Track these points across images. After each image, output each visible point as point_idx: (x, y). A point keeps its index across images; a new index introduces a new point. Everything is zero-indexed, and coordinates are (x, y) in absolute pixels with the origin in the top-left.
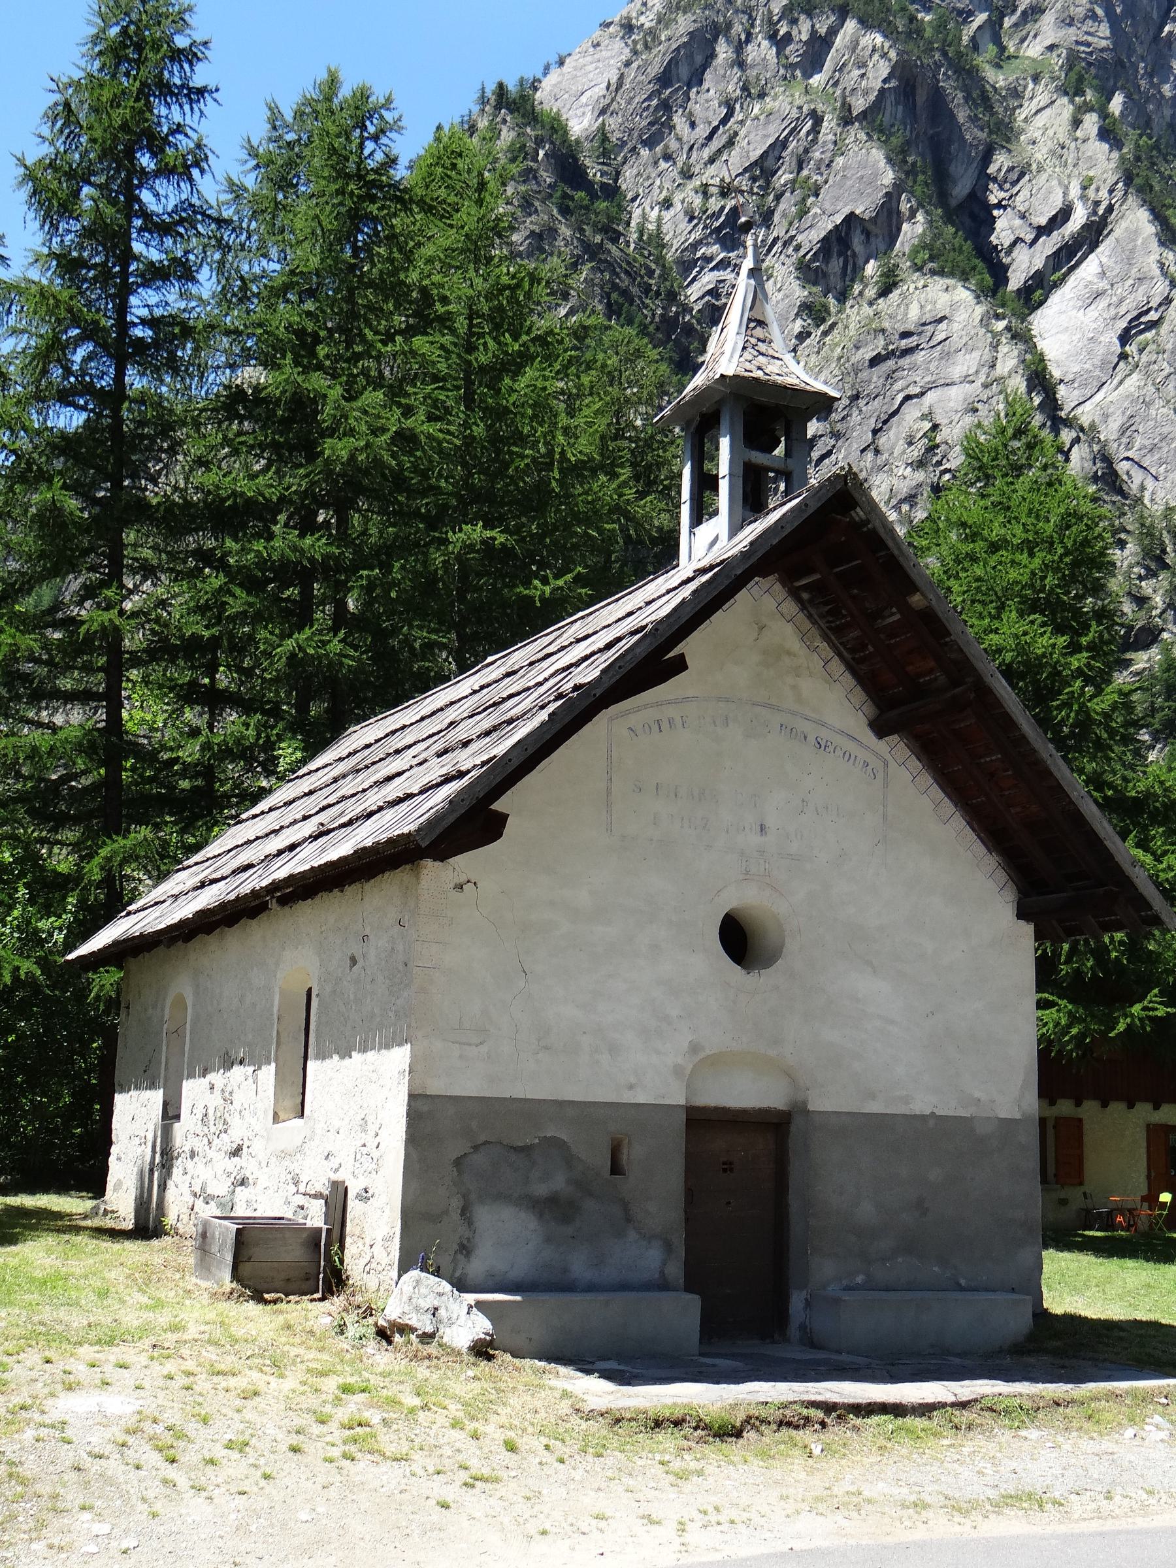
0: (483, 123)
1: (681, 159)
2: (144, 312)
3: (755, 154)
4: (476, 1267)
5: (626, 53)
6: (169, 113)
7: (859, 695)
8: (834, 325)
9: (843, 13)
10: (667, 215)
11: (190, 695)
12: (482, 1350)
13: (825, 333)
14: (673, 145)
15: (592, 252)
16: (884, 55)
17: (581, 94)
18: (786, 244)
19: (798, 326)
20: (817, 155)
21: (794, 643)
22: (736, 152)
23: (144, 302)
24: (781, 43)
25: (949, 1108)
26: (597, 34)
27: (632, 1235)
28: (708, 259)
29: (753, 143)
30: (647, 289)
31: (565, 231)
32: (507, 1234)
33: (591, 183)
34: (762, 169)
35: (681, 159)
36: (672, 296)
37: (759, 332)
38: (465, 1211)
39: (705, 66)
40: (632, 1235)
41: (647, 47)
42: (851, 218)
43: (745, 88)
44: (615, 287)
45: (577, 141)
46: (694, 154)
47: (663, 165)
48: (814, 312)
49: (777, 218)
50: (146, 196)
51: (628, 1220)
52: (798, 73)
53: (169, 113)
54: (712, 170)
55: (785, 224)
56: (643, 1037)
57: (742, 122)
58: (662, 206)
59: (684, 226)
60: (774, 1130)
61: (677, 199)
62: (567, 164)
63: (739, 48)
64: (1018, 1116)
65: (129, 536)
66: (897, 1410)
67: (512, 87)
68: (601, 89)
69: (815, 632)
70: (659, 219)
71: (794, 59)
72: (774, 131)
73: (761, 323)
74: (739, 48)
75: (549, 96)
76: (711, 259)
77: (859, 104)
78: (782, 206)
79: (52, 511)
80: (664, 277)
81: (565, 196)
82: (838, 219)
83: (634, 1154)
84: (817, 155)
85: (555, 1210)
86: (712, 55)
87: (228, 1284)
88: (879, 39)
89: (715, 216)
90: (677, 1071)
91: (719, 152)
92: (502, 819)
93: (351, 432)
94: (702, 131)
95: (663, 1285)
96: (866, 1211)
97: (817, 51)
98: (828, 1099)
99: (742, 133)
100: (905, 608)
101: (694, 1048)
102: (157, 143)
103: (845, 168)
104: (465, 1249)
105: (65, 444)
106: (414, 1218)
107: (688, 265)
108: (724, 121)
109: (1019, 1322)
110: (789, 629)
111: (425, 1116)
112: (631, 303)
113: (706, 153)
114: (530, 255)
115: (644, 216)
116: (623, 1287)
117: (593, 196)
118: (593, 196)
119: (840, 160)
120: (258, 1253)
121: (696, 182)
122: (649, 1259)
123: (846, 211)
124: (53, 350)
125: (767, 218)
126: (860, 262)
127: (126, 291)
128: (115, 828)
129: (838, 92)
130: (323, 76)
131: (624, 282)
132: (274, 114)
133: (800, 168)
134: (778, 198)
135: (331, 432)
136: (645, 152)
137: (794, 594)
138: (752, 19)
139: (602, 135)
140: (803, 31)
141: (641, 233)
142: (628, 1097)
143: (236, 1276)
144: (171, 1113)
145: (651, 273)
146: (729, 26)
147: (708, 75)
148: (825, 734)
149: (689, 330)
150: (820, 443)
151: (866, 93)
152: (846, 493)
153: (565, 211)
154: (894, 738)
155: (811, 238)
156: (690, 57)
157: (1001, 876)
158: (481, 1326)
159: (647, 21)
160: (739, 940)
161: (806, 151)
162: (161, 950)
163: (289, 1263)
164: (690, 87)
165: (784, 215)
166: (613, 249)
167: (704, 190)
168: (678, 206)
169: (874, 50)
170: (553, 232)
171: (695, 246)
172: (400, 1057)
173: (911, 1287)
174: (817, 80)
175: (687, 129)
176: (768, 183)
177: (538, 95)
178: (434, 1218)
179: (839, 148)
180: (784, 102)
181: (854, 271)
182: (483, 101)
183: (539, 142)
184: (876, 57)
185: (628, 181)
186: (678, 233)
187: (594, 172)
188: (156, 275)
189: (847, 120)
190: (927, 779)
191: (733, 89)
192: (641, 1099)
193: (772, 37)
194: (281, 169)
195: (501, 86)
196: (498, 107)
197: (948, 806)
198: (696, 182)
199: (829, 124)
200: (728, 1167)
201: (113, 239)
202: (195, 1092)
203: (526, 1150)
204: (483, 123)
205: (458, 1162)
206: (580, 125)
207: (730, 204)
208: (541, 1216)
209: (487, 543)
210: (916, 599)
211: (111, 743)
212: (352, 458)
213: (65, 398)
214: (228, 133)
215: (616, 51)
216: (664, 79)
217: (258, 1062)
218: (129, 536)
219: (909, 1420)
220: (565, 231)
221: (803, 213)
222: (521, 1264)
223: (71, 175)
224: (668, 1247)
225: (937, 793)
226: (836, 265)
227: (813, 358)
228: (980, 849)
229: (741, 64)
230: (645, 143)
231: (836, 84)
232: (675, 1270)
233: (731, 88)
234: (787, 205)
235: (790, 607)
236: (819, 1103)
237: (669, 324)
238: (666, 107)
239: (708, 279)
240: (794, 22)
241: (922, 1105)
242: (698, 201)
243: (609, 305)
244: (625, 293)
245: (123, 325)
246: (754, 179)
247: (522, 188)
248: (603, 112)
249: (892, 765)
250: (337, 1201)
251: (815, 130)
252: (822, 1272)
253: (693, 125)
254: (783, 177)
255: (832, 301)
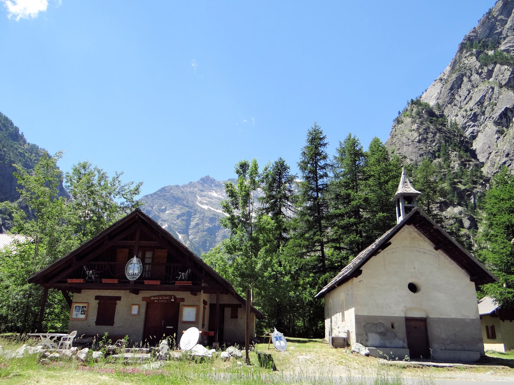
0: (409, 108)
1: (459, 105)
2: (320, 183)
3: (478, 100)
4: (369, 343)
5: (442, 85)
6: (321, 149)
7: (431, 243)
8: (506, 135)
9: (495, 63)
10: (457, 118)
11: (336, 248)
12: (367, 355)
13: (504, 137)
14: (456, 102)
15: (439, 130)
16: (508, 70)
17: (431, 98)
18: (490, 118)
19: (496, 136)
20: (494, 96)
21: (417, 236)
22: (472, 100)
23: (320, 182)
24: (480, 74)
25: (459, 317)
26: (434, 83)
27: (397, 339)
28: (469, 125)
29: (477, 97)
30: (455, 135)
31: (432, 127)
32: (374, 339)
33: (437, 115)
34: (480, 103)
35: (459, 105)
36: (461, 136)
37: (406, 184)
38: (366, 334)
39: (461, 84)
40: (397, 339)
41: (446, 83)
42: (506, 109)
43: (473, 86)
44: (446, 136)
45: (432, 107)
46: (462, 103)
47: (454, 107)
48: (500, 132)
49: (486, 113)
50: (319, 163)
51: (396, 336)
52: (486, 79)
53: (321, 149)
54: (467, 105)
55: (489, 113)
56: (397, 305)
57: (473, 94)
58: (455, 117)
59: (462, 119)
60: (424, 321)
61: (459, 114)
62: (431, 113)
63: (469, 77)
64: (475, 318)
65: (322, 222)
66: (437, 367)
67: (415, 99)
68: (436, 94)
69: (421, 233)
70: (455, 119)
71: (484, 77)
72: (482, 94)
73: (406, 182)
74: (469, 77)
75: (424, 100)
76: (470, 125)
77: (504, 83)
78: (487, 109)
79: (308, 220)
80: (458, 132)
81: (431, 119)
82: (503, 110)
83: (396, 325)
84: (494, 96)
85: (382, 334)
86: (463, 81)
87: (331, 346)
88: (506, 67)
89: (470, 115)
90: (402, 311)
91: (468, 101)
92: (362, 271)
93: (356, 199)
94: (463, 98)
95: (403, 347)
96: (443, 336)
97: (490, 74)
98: (433, 315)
99: (473, 96)
100: (433, 229)
101: (405, 307)
102: (320, 154)
103: (502, 98)
104: (367, 340)
105: (309, 208)
106: (358, 335)
107: (464, 128)
108: (468, 94)
109: (477, 356)
110: (416, 233)
111: (358, 319)
112: (451, 139)
113: (465, 102)
114: (424, 134)
115: (451, 119)
116: (396, 348)
117: (438, 118)
118: (438, 118)
119: (501, 96)
120: (336, 341)
121: (464, 109)
122: (401, 343)
123: (505, 107)
124: (306, 193)
125: (483, 113)
126: (511, 118)
127: (316, 181)
128: (324, 273)
129: (497, 81)
130: (348, 135)
131: (448, 135)
132: (340, 143)
133: (490, 100)
134: (486, 108)
135: (353, 200)
136: (449, 105)
137: (416, 227)
138: (471, 71)
139: (438, 104)
140: (485, 69)
141: (451, 123)
142: (393, 315)
143: (333, 345)
144: (331, 321)
145: (455, 131)
146: (466, 73)
147: (462, 85)
148: (425, 251)
149: (467, 142)
150: (507, 163)
151: (505, 79)
152: (417, 213)
153: (431, 122)
154: (439, 250)
155: (496, 115)
156: (457, 83)
157: (466, 273)
158: (367, 351)
159: (445, 77)
160: (413, 288)
161: (491, 96)
162: (327, 295)
163: (345, 343)
164: (458, 89)
165: (488, 112)
166: (444, 128)
167: (466, 111)
168: (460, 115)
169: (505, 69)
170: (429, 128)
171: (466, 123)
172: (353, 310)
173: (454, 350)
174: (491, 80)
175: (459, 98)
176: (482, 105)
177: (421, 99)
178: (361, 335)
179: (500, 94)
180: (483, 87)
181: (510, 120)
182: (408, 104)
183: (423, 109)
184: (506, 71)
185: (446, 113)
186: (460, 121)
187: (437, 113)
188: (321, 177)
189: (501, 87)
190: (447, 257)
191: (469, 87)
192: (396, 316)
193: (478, 73)
194: (342, 152)
195: (412, 100)
196: (412, 104)
197: (453, 261)
198: (464, 109)
199: (496, 89)
200: (416, 328)
201: (315, 172)
202: (333, 317)
203: (376, 324)
204: (409, 108)
205: (364, 326)
206: (432, 103)
207: (473, 112)
208: (380, 335)
209: (384, 216)
210: (434, 227)
211: (322, 258)
212: (357, 205)
213: (309, 200)
214: (331, 151)
215: (439, 85)
216: (451, 89)
217: (339, 312)
218: (322, 222)
219: (439, 368)
220: (432, 127)
221: (493, 110)
222: (377, 343)
223: (306, 163)
224: (404, 341)
225: (450, 259)
226: (504, 120)
227: (502, 143)
228: (460, 269)
229: (470, 81)
230: (449, 104)
231: (496, 79)
232: (406, 345)
233: (469, 87)
234: (488, 109)
235: (416, 230)
236: (431, 316)
237: (462, 142)
238: (453, 94)
239: (470, 130)
240: (483, 68)
241: (453, 316)
242: (464, 113)
243: (445, 141)
244: (449, 137)
245: (317, 186)
246: (478, 105)
247: (420, 120)
248: (438, 99)
249: (440, 255)
250: (348, 333)
251: (493, 91)
252: (435, 347)
253: (460, 97)
254: (486, 103)
255: (505, 129)
